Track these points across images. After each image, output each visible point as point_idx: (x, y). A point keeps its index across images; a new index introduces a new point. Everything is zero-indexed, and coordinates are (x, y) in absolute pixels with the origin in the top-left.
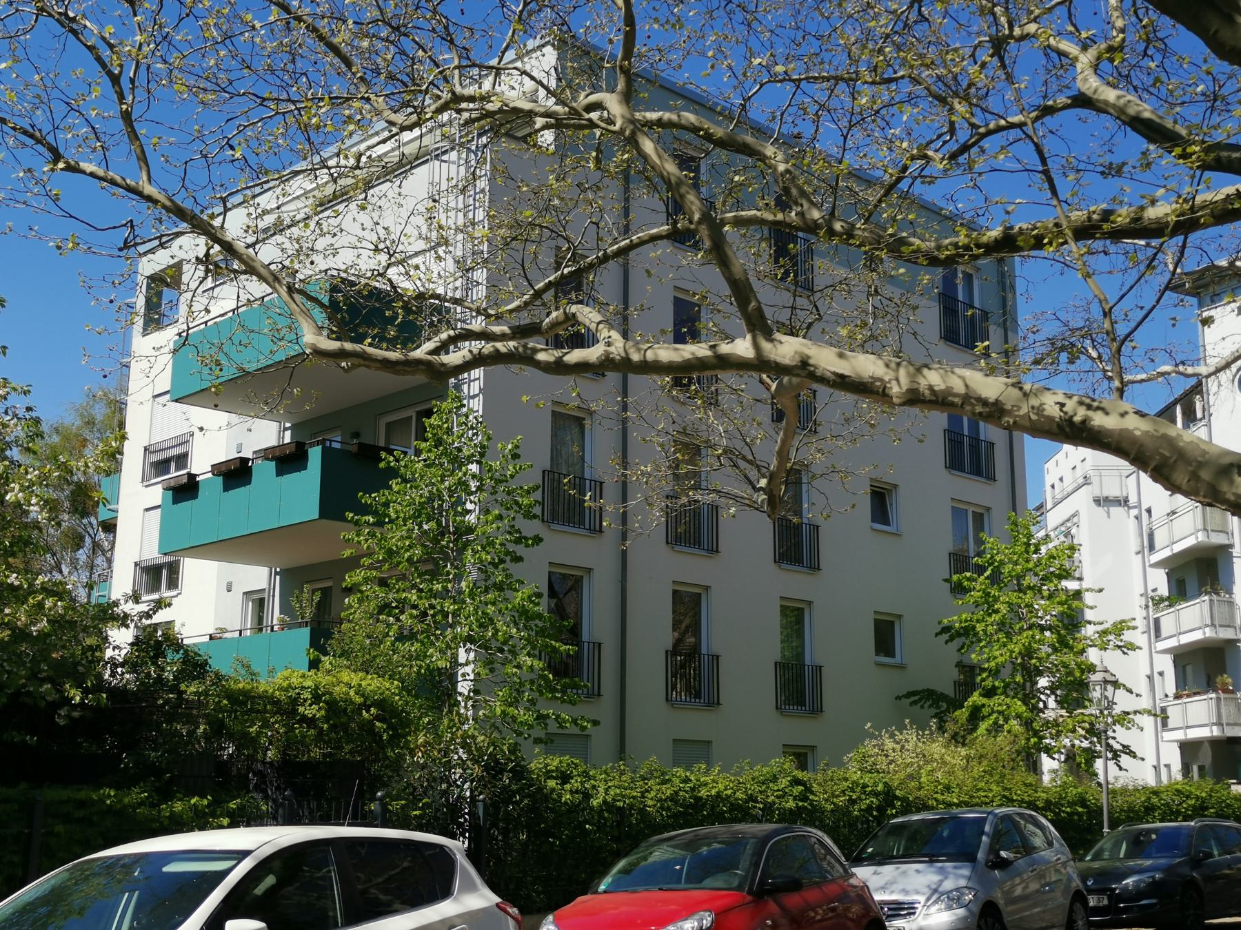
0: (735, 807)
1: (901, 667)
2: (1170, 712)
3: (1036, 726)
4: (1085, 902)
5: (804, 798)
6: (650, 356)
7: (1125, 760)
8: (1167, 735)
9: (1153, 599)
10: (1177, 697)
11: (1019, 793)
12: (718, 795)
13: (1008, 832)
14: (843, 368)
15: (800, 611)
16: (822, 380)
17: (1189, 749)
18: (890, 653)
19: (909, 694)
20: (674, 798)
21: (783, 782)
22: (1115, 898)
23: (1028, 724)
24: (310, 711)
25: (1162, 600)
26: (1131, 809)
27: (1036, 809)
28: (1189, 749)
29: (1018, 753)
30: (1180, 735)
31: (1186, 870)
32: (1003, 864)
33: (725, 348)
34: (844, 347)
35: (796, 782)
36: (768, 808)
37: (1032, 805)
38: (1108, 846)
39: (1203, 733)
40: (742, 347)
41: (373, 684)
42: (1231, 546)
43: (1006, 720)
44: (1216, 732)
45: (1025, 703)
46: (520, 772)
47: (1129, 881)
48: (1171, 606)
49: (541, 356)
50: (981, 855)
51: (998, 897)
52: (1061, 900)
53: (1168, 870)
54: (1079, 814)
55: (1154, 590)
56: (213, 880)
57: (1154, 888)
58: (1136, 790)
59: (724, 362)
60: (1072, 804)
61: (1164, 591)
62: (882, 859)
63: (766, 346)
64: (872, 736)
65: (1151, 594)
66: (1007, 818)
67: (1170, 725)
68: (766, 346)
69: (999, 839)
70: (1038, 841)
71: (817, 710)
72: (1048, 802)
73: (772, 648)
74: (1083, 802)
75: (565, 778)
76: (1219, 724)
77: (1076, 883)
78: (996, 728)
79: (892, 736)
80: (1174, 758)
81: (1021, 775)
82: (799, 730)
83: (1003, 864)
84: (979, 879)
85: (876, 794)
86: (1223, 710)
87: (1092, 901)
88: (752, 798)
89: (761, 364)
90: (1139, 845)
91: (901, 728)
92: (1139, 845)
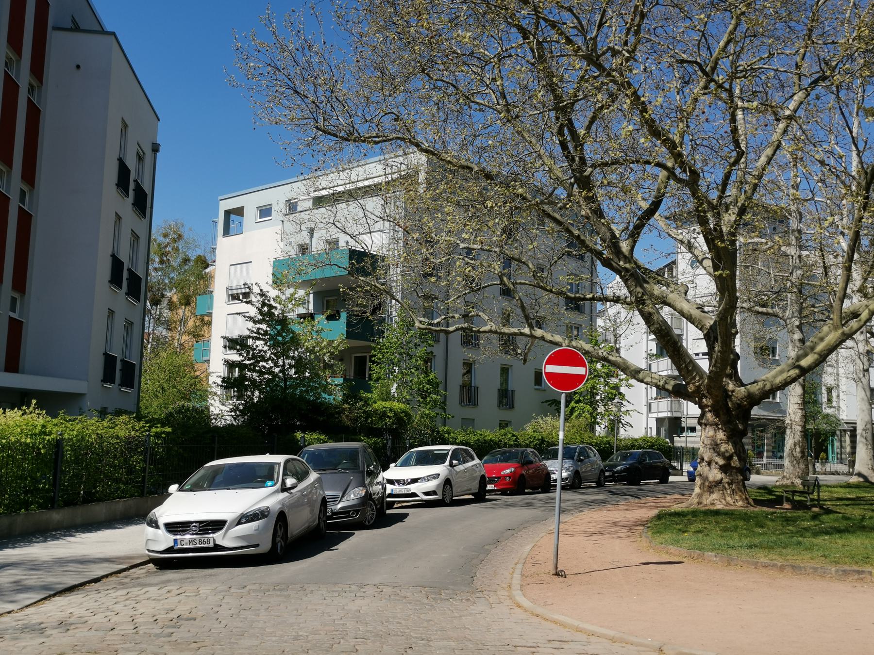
0: (495, 443)
1: (544, 390)
2: (652, 404)
3: (594, 414)
4: (604, 474)
5: (516, 441)
6: (502, 331)
7: (628, 428)
8: (651, 415)
9: (649, 354)
10: (656, 399)
11: (587, 440)
12: (491, 440)
13: (583, 452)
14: (552, 339)
15: (507, 369)
16: (546, 341)
17: (660, 421)
18: (540, 385)
19: (547, 401)
20: (478, 440)
21: (510, 435)
22: (614, 473)
23: (591, 414)
24: (390, 414)
25: (653, 355)
26: (626, 446)
27: (592, 445)
28: (660, 421)
29: (587, 425)
30: (655, 415)
31: (637, 465)
32: (581, 461)
33: (522, 331)
34: (553, 332)
35: (513, 435)
36: (505, 444)
37: (591, 444)
38: (615, 458)
39: (664, 415)
40: (527, 330)
41: (402, 406)
42: (682, 335)
43: (584, 412)
44: (669, 415)
45: (591, 406)
46: (438, 432)
47: (619, 468)
48: (657, 358)
49: (474, 329)
50: (575, 458)
51: (579, 469)
52: (597, 472)
53: (630, 465)
54: (607, 448)
55: (651, 350)
56: (447, 454)
57: (626, 470)
58: (629, 439)
59: (522, 334)
60: (605, 444)
61: (654, 352)
62: (548, 459)
63: (533, 332)
64: (535, 419)
65: (649, 352)
66: (583, 448)
67: (652, 411)
68: (533, 332)
69: (580, 454)
70: (592, 455)
71: (512, 407)
72: (596, 443)
73: (496, 384)
74: (609, 443)
75: (449, 433)
76: (671, 411)
77: (602, 467)
78: (580, 415)
79: (542, 419)
80: (653, 424)
81: (587, 434)
82: (506, 415)
83: (581, 461)
84: (575, 465)
85: (538, 440)
86: (673, 406)
87: (607, 474)
88: (500, 441)
89: (532, 336)
90: (625, 458)
91: (546, 416)
92: (625, 458)
